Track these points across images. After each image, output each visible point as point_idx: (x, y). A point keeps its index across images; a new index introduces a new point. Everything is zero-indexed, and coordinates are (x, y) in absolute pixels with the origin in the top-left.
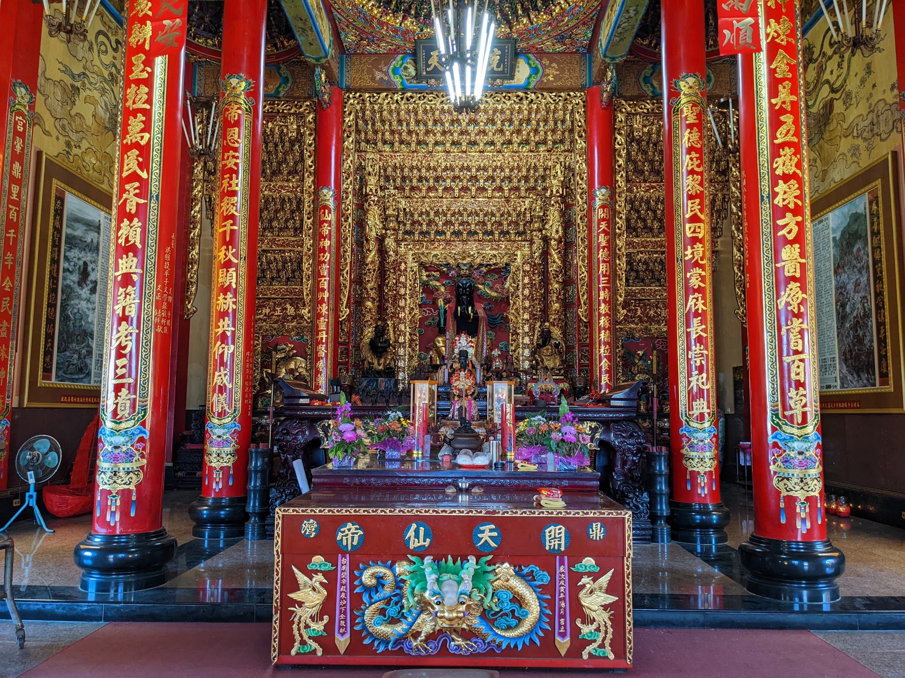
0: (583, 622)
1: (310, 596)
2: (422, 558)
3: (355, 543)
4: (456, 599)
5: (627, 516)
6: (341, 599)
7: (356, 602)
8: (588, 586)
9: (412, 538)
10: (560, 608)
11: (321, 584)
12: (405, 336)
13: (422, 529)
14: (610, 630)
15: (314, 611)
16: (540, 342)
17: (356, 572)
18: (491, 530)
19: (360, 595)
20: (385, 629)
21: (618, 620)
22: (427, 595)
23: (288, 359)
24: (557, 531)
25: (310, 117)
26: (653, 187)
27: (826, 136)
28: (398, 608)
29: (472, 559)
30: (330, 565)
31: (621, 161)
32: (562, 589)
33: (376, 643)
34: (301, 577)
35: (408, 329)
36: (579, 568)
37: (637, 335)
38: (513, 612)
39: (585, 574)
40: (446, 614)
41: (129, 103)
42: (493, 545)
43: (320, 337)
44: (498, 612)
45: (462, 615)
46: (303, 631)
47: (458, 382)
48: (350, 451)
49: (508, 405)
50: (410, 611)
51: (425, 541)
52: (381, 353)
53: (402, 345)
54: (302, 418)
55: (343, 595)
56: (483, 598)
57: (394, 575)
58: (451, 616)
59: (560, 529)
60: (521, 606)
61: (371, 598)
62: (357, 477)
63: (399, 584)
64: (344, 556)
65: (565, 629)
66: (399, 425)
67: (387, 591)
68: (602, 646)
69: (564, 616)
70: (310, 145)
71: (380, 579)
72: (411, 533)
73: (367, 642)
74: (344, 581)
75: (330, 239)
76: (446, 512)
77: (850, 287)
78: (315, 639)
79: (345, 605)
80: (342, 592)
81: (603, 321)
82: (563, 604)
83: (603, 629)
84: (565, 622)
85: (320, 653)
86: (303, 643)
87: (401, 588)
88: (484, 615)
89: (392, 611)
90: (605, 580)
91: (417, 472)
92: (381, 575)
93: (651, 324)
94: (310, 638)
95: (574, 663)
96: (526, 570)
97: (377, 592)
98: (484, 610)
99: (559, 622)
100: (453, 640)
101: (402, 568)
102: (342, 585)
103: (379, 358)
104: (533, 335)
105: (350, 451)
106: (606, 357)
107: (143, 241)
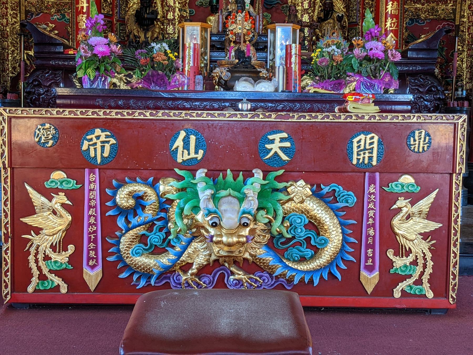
0: (396, 254)
2: (193, 172)
3: (106, 154)
4: (237, 220)
5: (460, 121)
6: (90, 224)
7: (109, 227)
8: (405, 210)
9: (180, 149)
10: (368, 236)
11: (63, 205)
12: (174, 12)
13: (193, 138)
14: (430, 264)
15: (56, 239)
16: (322, 15)
17: (108, 191)
18: (282, 140)
19: (114, 218)
21: (440, 252)
22: (199, 217)
24: (368, 141)
28: (162, 235)
29: (258, 174)
30: (73, 182)
32: (371, 213)
33: (135, 277)
34: (37, 198)
35: (177, 5)
36: (394, 187)
37: (423, 16)
38: (308, 240)
39: (401, 195)
40: (224, 239)
42: (285, 157)
43: (80, 5)
44: (289, 240)
45: (244, 239)
46: (41, 263)
47: (234, 26)
48: (102, 69)
49: (294, 45)
50: (177, 238)
51: (196, 152)
52: (148, 25)
53: (171, 22)
54: (55, 69)
55: (92, 220)
56: (270, 222)
57: (157, 195)
58: (230, 240)
59: (372, 138)
60: (318, 234)
61: (128, 222)
62: (113, 97)
63: (164, 204)
64: (92, 171)
65: (373, 262)
66: (165, 57)
67: (149, 214)
68: (419, 282)
69: (372, 246)
71: (139, 199)
72: (179, 143)
73: (123, 275)
74: (93, 204)
76: (224, 115)
78: (56, 273)
79: (95, 232)
80: (91, 216)
82: (371, 232)
83: (421, 261)
84: (374, 253)
85: (64, 289)
86: (42, 277)
87: (166, 211)
88: (271, 245)
89: (155, 238)
90: (425, 204)
91: (188, 92)
92: (141, 194)
93: (438, 5)
94: (51, 271)
95: (383, 302)
96: (326, 189)
97: (135, 215)
98: (273, 237)
99: (366, 253)
100: (233, 273)
101: (168, 186)
102: (90, 207)
103: (146, 31)
104: (313, 11)
105: (102, 69)
106: (392, 31)
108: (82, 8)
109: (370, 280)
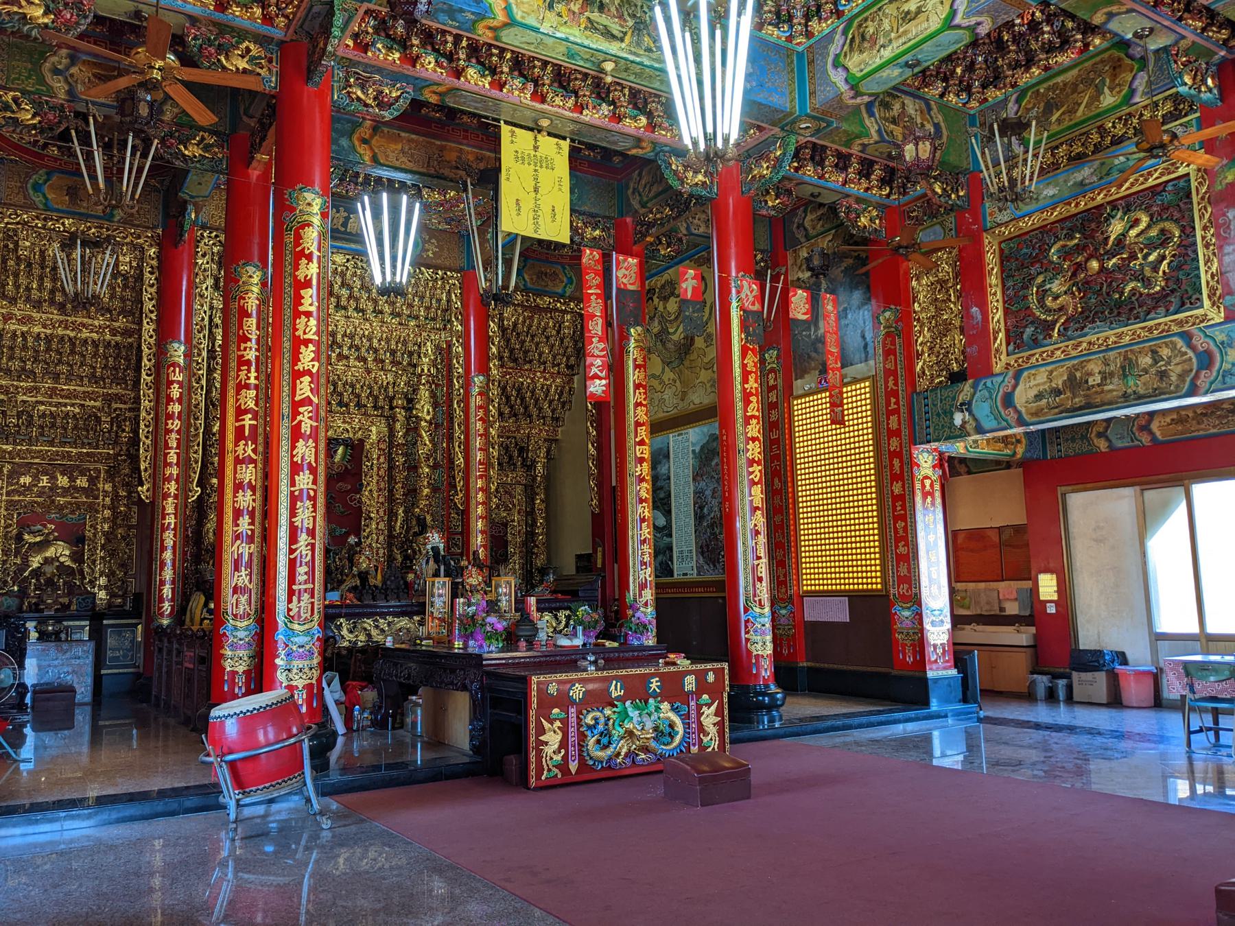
1: (553, 739)
7: (582, 737)
20: (600, 754)
23: (45, 544)
25: (152, 251)
26: (510, 374)
27: (687, 363)
31: (494, 350)
41: (299, 333)
67: (601, 727)
70: (152, 286)
71: (596, 719)
72: (613, 687)
75: (180, 404)
77: (708, 493)
80: (572, 731)
81: (480, 510)
89: (605, 741)
90: (713, 708)
107: (316, 461)
108: (169, 524)
109: (694, 749)
